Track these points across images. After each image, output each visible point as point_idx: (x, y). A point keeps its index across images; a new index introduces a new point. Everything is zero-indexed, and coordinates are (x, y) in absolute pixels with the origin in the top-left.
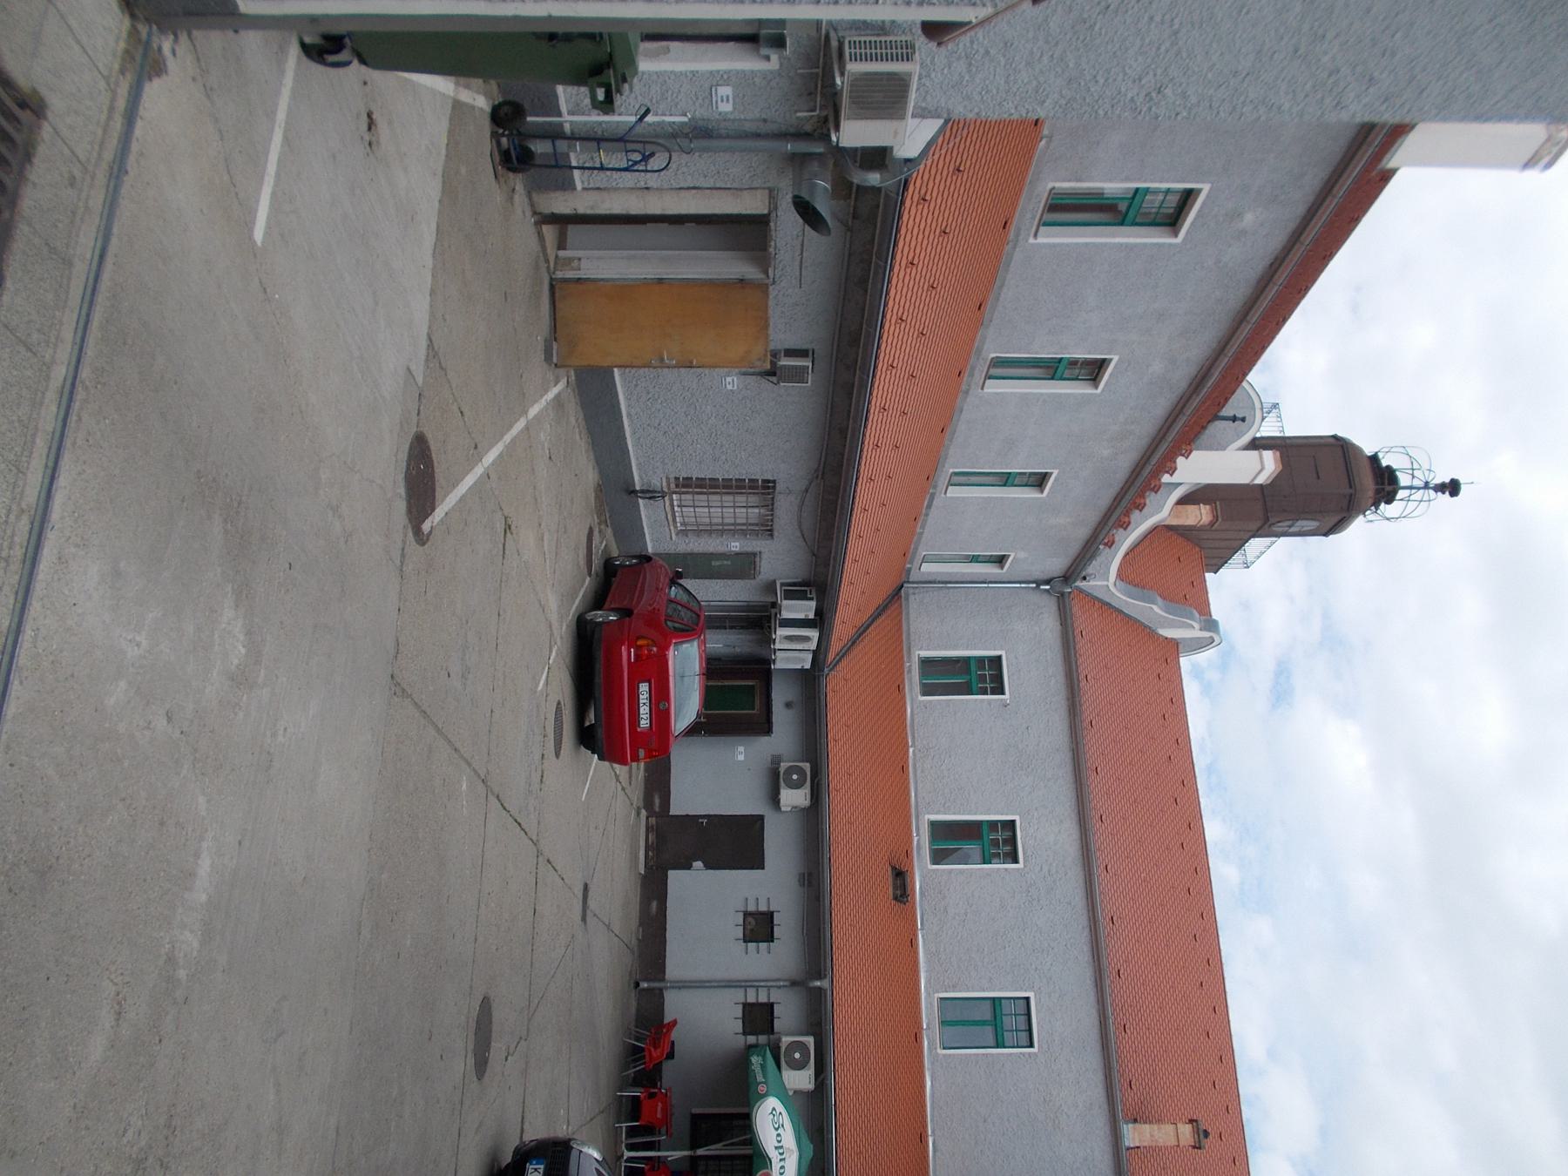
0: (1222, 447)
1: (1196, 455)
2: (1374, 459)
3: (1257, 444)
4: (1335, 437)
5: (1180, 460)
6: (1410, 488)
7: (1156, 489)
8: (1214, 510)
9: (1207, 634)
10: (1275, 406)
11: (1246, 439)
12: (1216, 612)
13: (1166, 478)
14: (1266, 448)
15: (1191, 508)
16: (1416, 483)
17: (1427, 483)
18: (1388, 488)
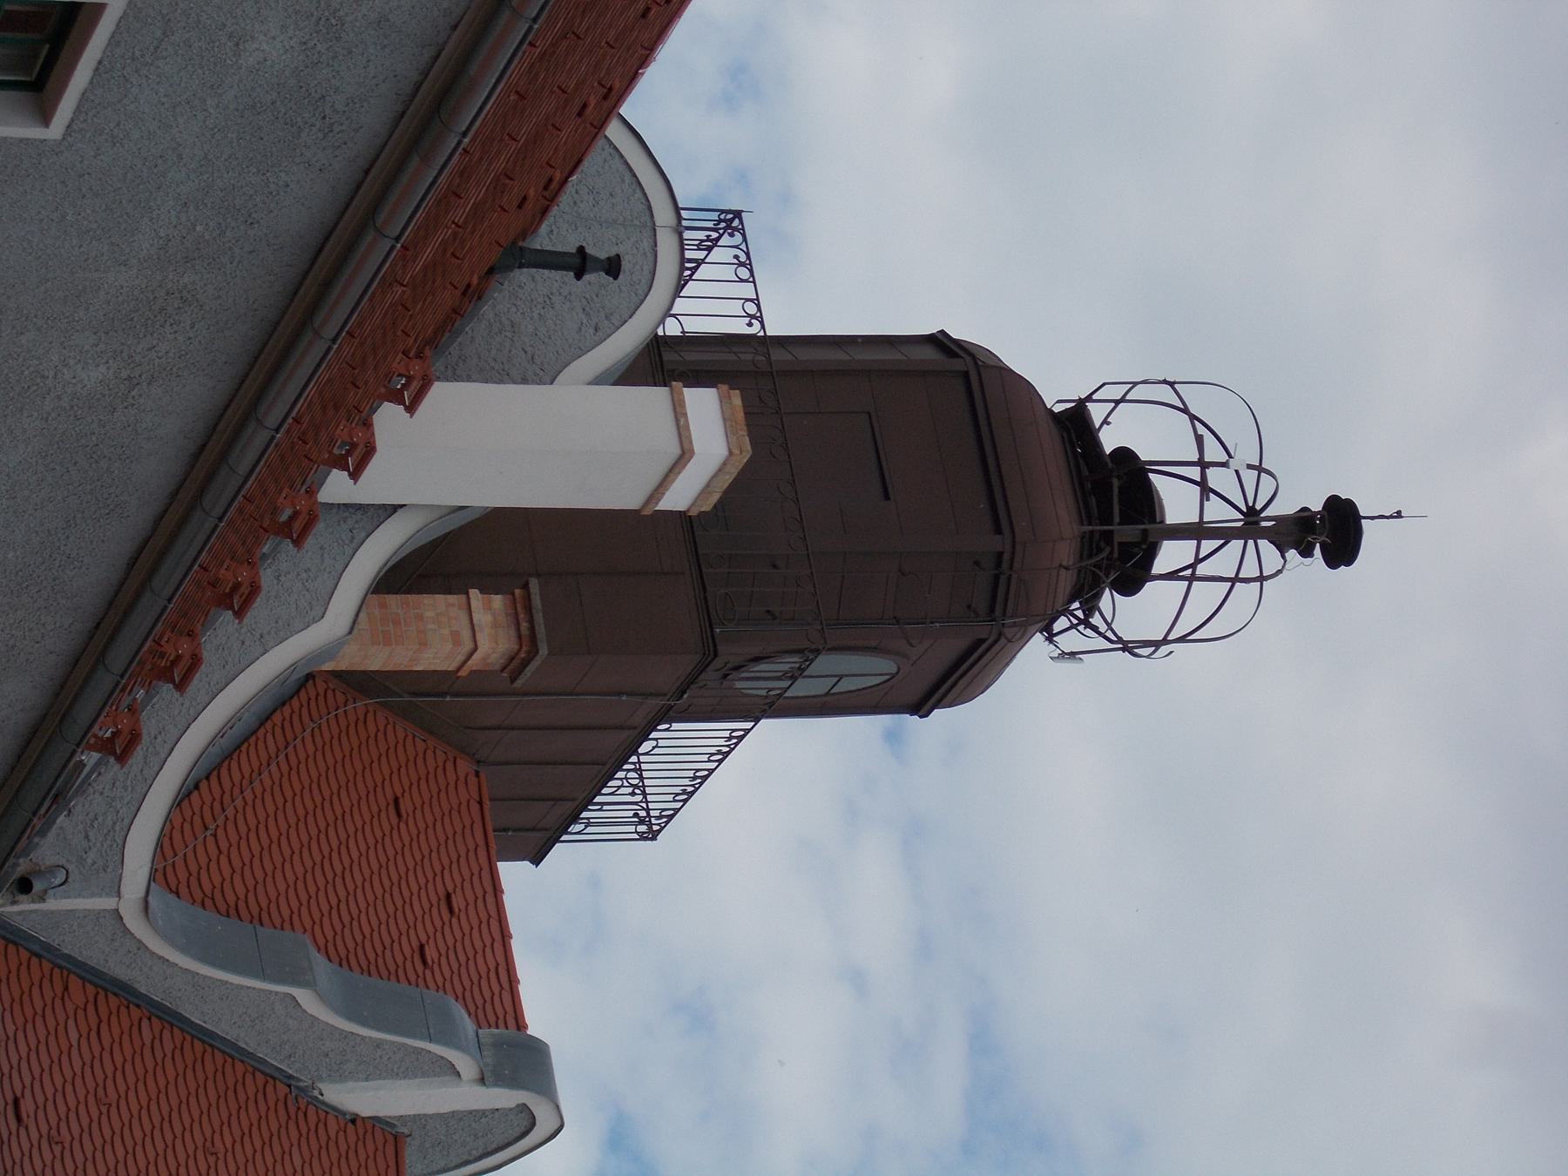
0: (540, 370)
1: (446, 398)
2: (1076, 424)
3: (666, 363)
4: (940, 342)
5: (388, 417)
6: (1196, 531)
7: (298, 529)
8: (521, 613)
9: (503, 1098)
10: (731, 221)
11: (625, 341)
12: (544, 1007)
13: (337, 487)
14: (699, 377)
15: (437, 607)
16: (1217, 512)
17: (1251, 514)
18: (1126, 533)
